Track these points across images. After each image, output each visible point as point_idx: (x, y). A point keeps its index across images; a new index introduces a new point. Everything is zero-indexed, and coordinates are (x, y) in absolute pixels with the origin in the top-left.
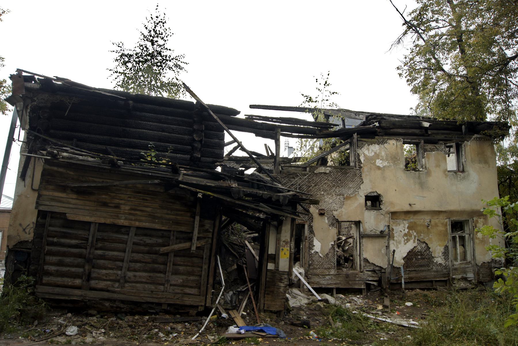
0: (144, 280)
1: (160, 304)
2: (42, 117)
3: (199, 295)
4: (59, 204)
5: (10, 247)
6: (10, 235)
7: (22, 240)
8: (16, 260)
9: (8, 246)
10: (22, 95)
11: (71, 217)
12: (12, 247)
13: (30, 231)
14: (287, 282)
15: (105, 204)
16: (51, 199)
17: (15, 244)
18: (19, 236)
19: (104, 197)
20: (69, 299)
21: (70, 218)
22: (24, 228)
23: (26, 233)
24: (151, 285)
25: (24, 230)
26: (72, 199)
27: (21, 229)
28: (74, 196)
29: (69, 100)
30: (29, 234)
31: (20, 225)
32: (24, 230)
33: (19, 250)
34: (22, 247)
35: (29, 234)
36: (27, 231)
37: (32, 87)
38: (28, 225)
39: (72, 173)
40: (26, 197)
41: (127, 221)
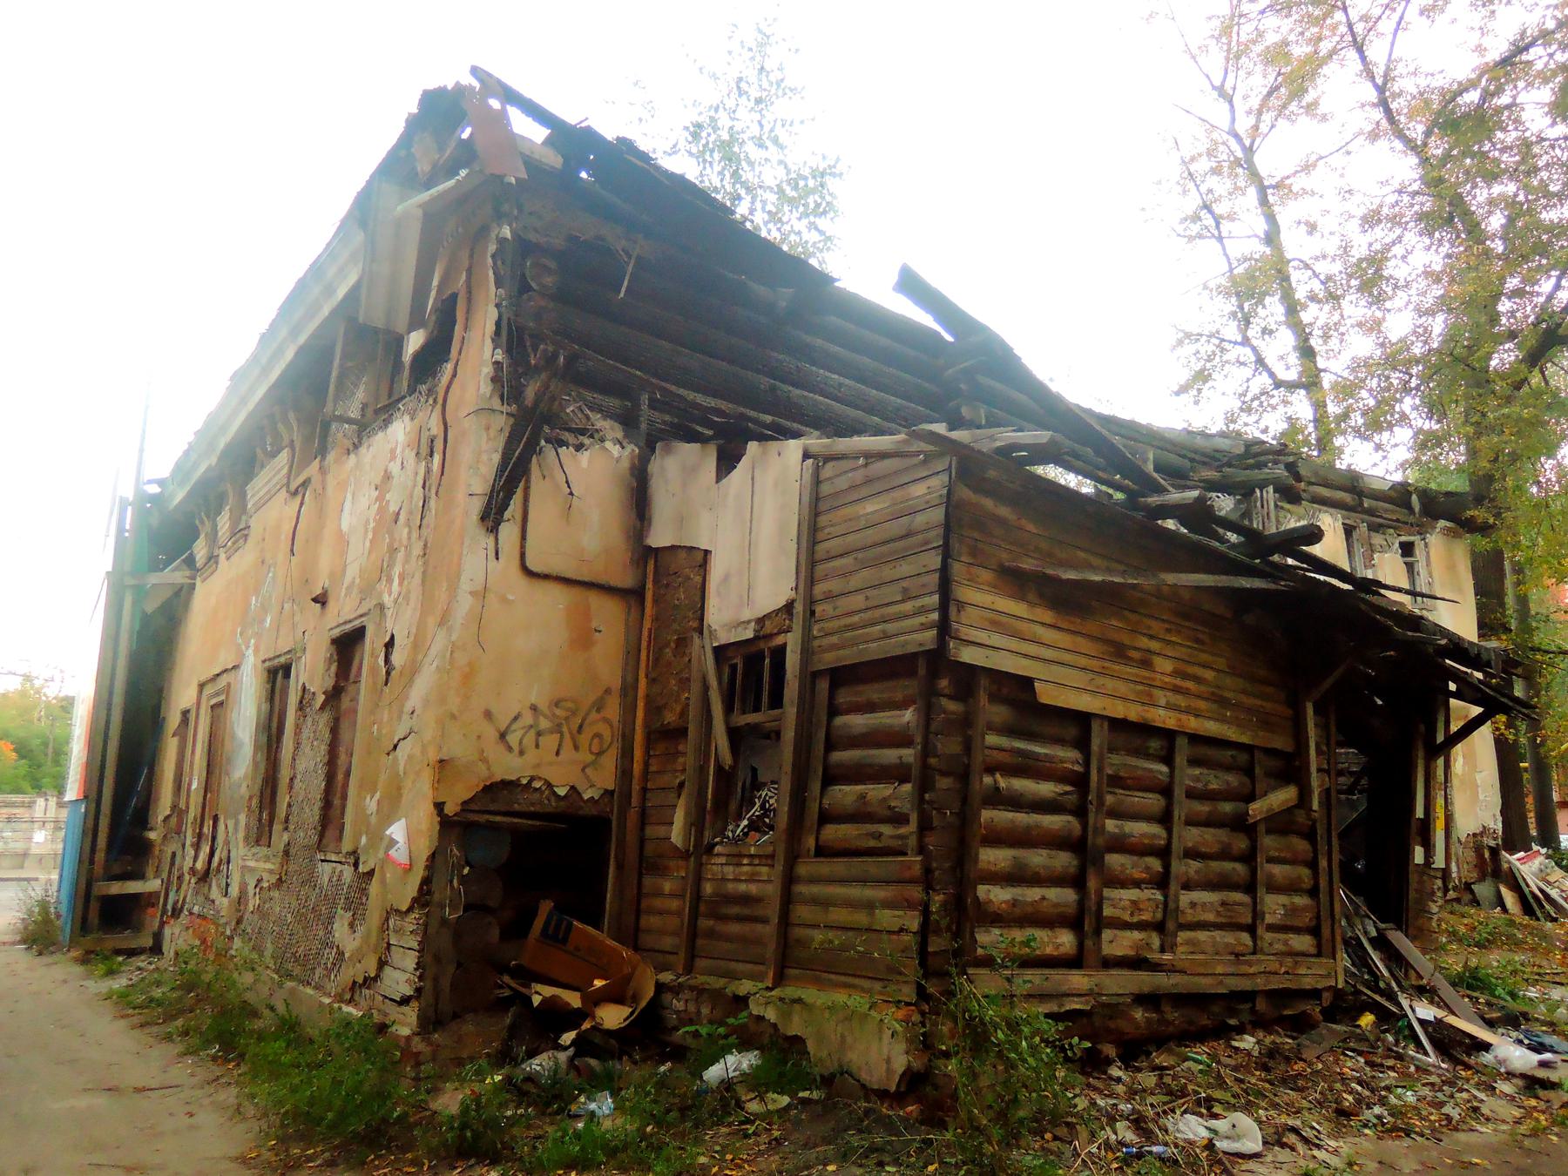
0: (1210, 917)
1: (1248, 996)
2: (533, 285)
3: (1319, 955)
4: (1013, 644)
5: (450, 809)
6: (452, 760)
7: (498, 778)
8: (468, 863)
9: (439, 806)
10: (517, 179)
11: (1047, 695)
12: (458, 809)
13: (524, 741)
14: (659, 893)
15: (1119, 652)
16: (994, 623)
17: (468, 795)
18: (485, 760)
19: (1114, 626)
20: (1063, 1010)
21: (1045, 699)
22: (502, 730)
23: (510, 749)
24: (1223, 933)
25: (503, 736)
26: (1043, 624)
27: (491, 733)
28: (1048, 616)
29: (624, 242)
30: (521, 753)
31: (488, 715)
32: (503, 736)
33: (483, 818)
34: (492, 807)
35: (521, 753)
36: (513, 739)
37: (537, 156)
38: (516, 719)
39: (1031, 527)
40: (504, 600)
41: (1170, 714)
